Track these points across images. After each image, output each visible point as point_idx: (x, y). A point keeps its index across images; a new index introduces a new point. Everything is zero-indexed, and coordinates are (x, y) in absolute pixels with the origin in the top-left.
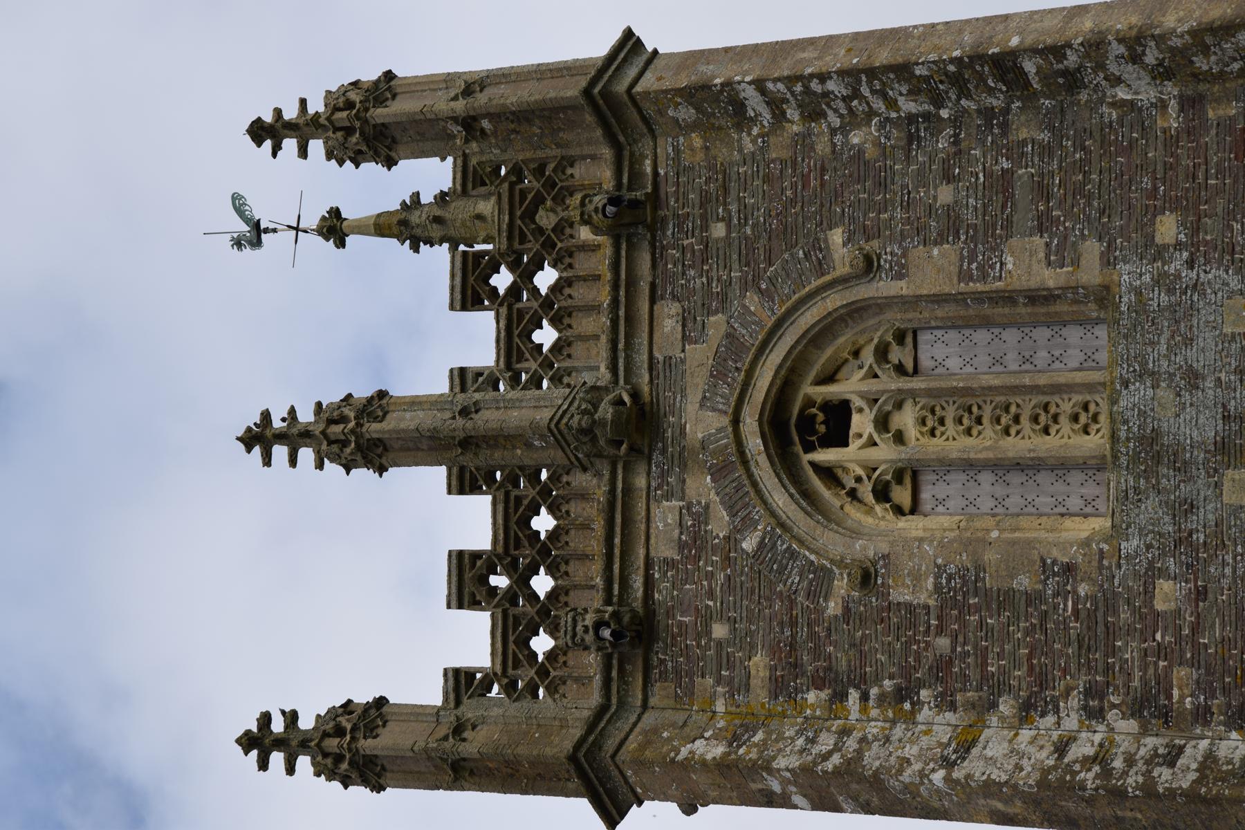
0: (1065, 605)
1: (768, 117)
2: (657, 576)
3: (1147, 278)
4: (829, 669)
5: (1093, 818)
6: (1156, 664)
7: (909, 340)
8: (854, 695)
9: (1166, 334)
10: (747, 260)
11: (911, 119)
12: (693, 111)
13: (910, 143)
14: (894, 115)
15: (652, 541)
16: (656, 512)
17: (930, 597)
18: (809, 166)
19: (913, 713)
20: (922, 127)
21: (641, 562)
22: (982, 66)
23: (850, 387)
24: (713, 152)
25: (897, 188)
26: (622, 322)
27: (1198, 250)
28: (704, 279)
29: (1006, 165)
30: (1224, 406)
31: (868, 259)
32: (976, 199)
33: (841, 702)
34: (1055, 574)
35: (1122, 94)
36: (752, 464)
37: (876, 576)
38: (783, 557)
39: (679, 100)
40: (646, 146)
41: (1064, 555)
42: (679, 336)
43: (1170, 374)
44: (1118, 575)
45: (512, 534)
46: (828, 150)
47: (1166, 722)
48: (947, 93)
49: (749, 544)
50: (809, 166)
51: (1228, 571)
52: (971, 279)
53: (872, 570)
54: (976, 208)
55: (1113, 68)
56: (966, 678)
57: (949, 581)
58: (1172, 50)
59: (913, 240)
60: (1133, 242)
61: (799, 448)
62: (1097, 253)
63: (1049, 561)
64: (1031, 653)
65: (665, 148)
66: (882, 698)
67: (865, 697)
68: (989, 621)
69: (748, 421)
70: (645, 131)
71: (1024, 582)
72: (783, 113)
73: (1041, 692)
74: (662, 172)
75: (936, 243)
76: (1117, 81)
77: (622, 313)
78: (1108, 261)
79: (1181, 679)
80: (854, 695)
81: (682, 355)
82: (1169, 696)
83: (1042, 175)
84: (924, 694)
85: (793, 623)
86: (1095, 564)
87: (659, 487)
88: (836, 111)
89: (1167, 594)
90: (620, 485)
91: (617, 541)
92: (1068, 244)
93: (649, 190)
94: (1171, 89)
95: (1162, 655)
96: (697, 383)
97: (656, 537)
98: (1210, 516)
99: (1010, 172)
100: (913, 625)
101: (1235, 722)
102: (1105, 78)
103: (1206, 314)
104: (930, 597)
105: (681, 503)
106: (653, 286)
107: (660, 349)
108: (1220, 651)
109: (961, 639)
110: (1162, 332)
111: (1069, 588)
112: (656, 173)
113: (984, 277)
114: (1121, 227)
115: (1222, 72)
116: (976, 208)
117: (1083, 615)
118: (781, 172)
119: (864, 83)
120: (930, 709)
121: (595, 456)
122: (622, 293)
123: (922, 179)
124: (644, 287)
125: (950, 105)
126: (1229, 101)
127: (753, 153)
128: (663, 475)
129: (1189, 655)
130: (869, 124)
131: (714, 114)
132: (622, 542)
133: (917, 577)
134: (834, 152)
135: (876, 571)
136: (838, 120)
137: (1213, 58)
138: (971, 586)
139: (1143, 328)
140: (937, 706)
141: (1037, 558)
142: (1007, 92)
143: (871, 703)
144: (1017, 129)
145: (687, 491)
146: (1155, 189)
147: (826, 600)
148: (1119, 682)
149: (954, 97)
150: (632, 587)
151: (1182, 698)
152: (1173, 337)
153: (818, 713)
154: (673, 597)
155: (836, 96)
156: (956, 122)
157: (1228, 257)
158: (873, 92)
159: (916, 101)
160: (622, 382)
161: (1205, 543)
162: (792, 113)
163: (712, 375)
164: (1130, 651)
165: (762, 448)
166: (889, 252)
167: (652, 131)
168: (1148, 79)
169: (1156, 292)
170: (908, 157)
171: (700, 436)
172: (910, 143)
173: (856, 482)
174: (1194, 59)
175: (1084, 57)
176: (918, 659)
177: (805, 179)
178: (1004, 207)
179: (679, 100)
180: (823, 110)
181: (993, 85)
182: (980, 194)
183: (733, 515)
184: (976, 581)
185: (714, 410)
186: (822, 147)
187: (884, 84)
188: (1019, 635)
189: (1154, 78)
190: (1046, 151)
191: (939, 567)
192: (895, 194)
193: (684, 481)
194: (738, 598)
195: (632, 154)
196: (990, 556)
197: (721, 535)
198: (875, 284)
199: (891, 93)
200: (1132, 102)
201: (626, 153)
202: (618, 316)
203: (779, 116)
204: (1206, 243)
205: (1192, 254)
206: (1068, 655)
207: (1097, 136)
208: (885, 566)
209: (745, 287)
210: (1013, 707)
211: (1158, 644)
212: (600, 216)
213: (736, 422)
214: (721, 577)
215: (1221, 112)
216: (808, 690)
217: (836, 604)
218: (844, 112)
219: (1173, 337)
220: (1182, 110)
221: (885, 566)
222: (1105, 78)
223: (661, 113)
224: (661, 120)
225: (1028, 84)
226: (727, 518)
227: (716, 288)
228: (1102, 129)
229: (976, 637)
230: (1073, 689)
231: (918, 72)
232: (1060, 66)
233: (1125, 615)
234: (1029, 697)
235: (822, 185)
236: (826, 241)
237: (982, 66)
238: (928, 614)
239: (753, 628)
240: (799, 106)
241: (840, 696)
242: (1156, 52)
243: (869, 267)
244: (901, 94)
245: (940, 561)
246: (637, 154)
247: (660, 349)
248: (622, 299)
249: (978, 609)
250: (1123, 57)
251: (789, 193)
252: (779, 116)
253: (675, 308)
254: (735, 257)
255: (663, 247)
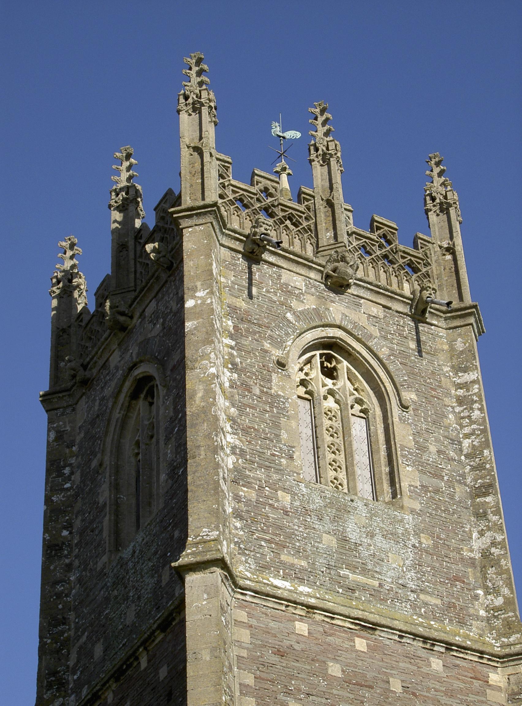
0: (276, 451)
1: (459, 381)
2: (274, 269)
3: (407, 526)
4: (242, 335)
5: (198, 436)
6: (256, 484)
7: (362, 415)
8: (233, 343)
9: (387, 529)
10: (401, 352)
11: (460, 443)
12: (461, 349)
13: (451, 440)
14: (461, 436)
15: (288, 272)
16: (300, 278)
17: (275, 391)
18: (439, 393)
19: (227, 367)
20: (457, 446)
21: (280, 264)
22: (489, 479)
23: (343, 382)
24: (442, 352)
25: (433, 428)
26: (378, 290)
27: (419, 551)
28: (392, 332)
29: (446, 478)
30: (361, 545)
31: (407, 408)
32: (432, 462)
33: (229, 336)
34: (289, 451)
35: (475, 535)
36: (323, 329)
37: (282, 370)
38: (286, 330)
39: (467, 345)
40: (442, 323)
41: (297, 457)
42: (370, 313)
43: (371, 525)
44: (291, 478)
45: (287, 209)
46: (446, 403)
47: (233, 481)
48: (474, 461)
49: (289, 315)
50: (439, 393)
51: (296, 527)
52: (402, 450)
53: (285, 369)
54: (429, 460)
55: (488, 534)
56: (244, 397)
57: (282, 402)
58: (499, 560)
59: (414, 429)
60: (420, 524)
61: (321, 352)
62: (415, 507)
63: (294, 449)
64: (256, 429)
65: (443, 333)
66: (231, 355)
67: (232, 348)
68: (267, 415)
69: (340, 333)
70: (449, 326)
71: (284, 435)
72: (461, 388)
73: (240, 428)
74: (433, 327)
75: (414, 439)
76: (481, 533)
77: (381, 291)
78: (412, 511)
79: (251, 492)
80: (233, 343)
81: (362, 312)
82: (243, 486)
83: (442, 492)
84: (235, 376)
85: (260, 326)
86: (294, 470)
87: (310, 283)
88: (463, 411)
89: (285, 499)
90: (314, 266)
91: (291, 256)
92: (418, 497)
93: (427, 320)
94: (478, 556)
95: (260, 488)
96: (353, 316)
97: (290, 275)
98: (317, 526)
99: (442, 479)
100: (263, 379)
101: (236, 512)
102: (482, 530)
103: (395, 548)
104: (275, 391)
105: (304, 291)
106: (390, 308)
107: (365, 303)
108: (264, 514)
109: (259, 399)
110: (387, 527)
111: (283, 455)
112: (432, 325)
113: (403, 456)
114: (426, 521)
115: (486, 578)
116: (429, 460)
117: (273, 458)
118: (437, 380)
119: (479, 427)
120: (230, 376)
121: (330, 259)
122: (389, 294)
123: (437, 440)
124: (389, 304)
125: (467, 461)
126: (475, 578)
127: (443, 370)
128: (316, 287)
129: (261, 500)
130: (456, 424)
131: (460, 358)
132: (291, 258)
133: (283, 388)
134: (445, 405)
135: (284, 370)
136: (457, 411)
137: (494, 576)
138: (281, 411)
139: (388, 519)
140: (231, 379)
141: (295, 445)
142: (475, 487)
143: (230, 350)
144: (459, 487)
145: (309, 295)
146: (441, 539)
147: (270, 343)
148: (247, 466)
149: (472, 464)
150: (270, 256)
151: (244, 491)
152: (386, 531)
153: (224, 324)
154: (266, 273)
155: (471, 413)
156: (460, 461)
157: (417, 562)
158: (474, 430)
159: (469, 446)
160: (355, 281)
161: (306, 521)
162: (461, 392)
163: (355, 323)
164: (260, 474)
165: (329, 335)
166: (409, 415)
167: (450, 329)
168: (483, 547)
169: (402, 529)
170: (445, 437)
171: (331, 309)
172: (451, 440)
173: (306, 373)
174: (494, 568)
175: (495, 523)
176: (249, 377)
177: (434, 390)
178: (430, 473)
179: (467, 345)
180: (463, 406)
181: (479, 481)
182: (434, 464)
183: (300, 312)
184: (283, 414)
185: (342, 319)
186: (447, 401)
187: (478, 435)
188: (262, 427)
189: (483, 550)
190: (452, 497)
191: (288, 399)
192: (432, 427)
193: (313, 295)
194: (267, 303)
195: (441, 317)
196: (293, 424)
197: (292, 304)
198: (397, 407)
199: (474, 437)
200: (471, 538)
201: (442, 314)
202: (380, 289)
203: (459, 386)
204: (422, 555)
205: (418, 548)
206: (256, 446)
207: (459, 520)
208: (285, 374)
209: (391, 349)
210: (233, 414)
211: (264, 488)
212: (428, 295)
213: (339, 327)
214: (275, 298)
215: (470, 574)
216: (233, 323)
217: (269, 348)
218: (462, 415)
219: (386, 531)
220: (471, 558)
221: (285, 374)
222: (482, 530)
223: (460, 335)
224: (455, 334)
225: (479, 496)
226: (299, 310)
227: (389, 336)
228: (461, 523)
229: (261, 407)
230: (243, 444)
231: (485, 451)
232: (489, 512)
233: (275, 477)
234: (238, 423)
235: (432, 396)
236: (411, 391)
237: (489, 479)
238: (268, 388)
239: (256, 306)
240: (465, 396)
241: (231, 337)
242: (498, 553)
243: (404, 407)
244: (472, 441)
245: (290, 400)
246: (440, 319)
247: (365, 303)
248: (387, 293)
249: (272, 411)
250: (495, 539)
251: (428, 380)
252: (459, 386)
253: (381, 315)
254: (402, 349)
255: (404, 318)
